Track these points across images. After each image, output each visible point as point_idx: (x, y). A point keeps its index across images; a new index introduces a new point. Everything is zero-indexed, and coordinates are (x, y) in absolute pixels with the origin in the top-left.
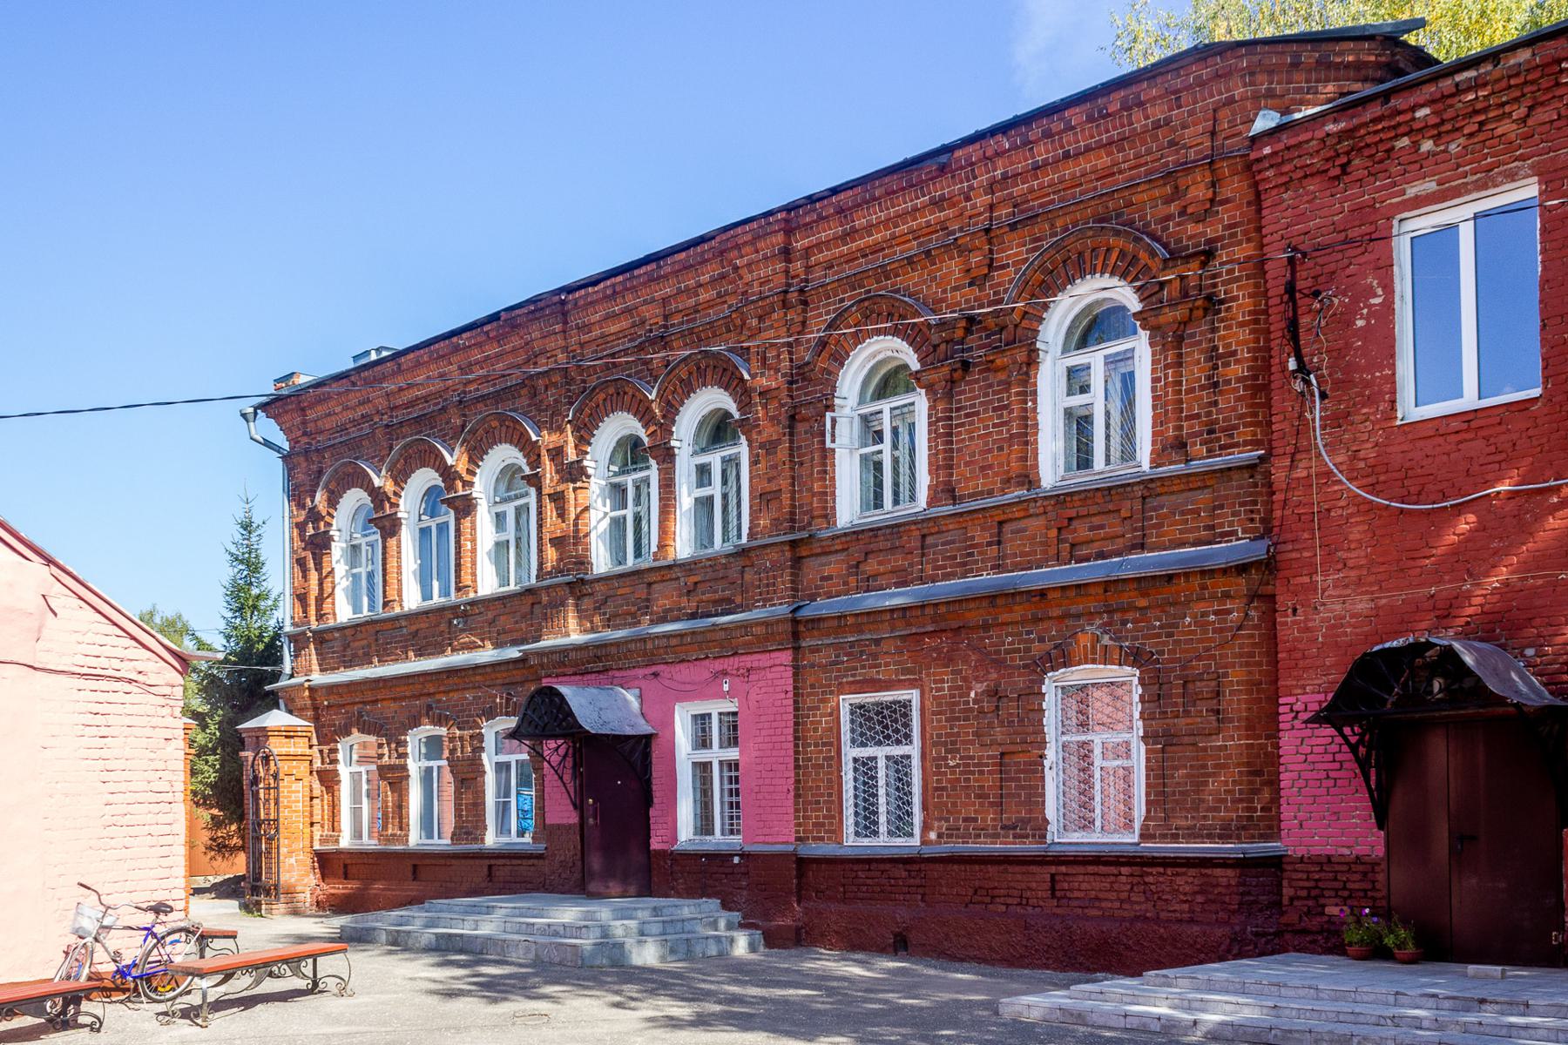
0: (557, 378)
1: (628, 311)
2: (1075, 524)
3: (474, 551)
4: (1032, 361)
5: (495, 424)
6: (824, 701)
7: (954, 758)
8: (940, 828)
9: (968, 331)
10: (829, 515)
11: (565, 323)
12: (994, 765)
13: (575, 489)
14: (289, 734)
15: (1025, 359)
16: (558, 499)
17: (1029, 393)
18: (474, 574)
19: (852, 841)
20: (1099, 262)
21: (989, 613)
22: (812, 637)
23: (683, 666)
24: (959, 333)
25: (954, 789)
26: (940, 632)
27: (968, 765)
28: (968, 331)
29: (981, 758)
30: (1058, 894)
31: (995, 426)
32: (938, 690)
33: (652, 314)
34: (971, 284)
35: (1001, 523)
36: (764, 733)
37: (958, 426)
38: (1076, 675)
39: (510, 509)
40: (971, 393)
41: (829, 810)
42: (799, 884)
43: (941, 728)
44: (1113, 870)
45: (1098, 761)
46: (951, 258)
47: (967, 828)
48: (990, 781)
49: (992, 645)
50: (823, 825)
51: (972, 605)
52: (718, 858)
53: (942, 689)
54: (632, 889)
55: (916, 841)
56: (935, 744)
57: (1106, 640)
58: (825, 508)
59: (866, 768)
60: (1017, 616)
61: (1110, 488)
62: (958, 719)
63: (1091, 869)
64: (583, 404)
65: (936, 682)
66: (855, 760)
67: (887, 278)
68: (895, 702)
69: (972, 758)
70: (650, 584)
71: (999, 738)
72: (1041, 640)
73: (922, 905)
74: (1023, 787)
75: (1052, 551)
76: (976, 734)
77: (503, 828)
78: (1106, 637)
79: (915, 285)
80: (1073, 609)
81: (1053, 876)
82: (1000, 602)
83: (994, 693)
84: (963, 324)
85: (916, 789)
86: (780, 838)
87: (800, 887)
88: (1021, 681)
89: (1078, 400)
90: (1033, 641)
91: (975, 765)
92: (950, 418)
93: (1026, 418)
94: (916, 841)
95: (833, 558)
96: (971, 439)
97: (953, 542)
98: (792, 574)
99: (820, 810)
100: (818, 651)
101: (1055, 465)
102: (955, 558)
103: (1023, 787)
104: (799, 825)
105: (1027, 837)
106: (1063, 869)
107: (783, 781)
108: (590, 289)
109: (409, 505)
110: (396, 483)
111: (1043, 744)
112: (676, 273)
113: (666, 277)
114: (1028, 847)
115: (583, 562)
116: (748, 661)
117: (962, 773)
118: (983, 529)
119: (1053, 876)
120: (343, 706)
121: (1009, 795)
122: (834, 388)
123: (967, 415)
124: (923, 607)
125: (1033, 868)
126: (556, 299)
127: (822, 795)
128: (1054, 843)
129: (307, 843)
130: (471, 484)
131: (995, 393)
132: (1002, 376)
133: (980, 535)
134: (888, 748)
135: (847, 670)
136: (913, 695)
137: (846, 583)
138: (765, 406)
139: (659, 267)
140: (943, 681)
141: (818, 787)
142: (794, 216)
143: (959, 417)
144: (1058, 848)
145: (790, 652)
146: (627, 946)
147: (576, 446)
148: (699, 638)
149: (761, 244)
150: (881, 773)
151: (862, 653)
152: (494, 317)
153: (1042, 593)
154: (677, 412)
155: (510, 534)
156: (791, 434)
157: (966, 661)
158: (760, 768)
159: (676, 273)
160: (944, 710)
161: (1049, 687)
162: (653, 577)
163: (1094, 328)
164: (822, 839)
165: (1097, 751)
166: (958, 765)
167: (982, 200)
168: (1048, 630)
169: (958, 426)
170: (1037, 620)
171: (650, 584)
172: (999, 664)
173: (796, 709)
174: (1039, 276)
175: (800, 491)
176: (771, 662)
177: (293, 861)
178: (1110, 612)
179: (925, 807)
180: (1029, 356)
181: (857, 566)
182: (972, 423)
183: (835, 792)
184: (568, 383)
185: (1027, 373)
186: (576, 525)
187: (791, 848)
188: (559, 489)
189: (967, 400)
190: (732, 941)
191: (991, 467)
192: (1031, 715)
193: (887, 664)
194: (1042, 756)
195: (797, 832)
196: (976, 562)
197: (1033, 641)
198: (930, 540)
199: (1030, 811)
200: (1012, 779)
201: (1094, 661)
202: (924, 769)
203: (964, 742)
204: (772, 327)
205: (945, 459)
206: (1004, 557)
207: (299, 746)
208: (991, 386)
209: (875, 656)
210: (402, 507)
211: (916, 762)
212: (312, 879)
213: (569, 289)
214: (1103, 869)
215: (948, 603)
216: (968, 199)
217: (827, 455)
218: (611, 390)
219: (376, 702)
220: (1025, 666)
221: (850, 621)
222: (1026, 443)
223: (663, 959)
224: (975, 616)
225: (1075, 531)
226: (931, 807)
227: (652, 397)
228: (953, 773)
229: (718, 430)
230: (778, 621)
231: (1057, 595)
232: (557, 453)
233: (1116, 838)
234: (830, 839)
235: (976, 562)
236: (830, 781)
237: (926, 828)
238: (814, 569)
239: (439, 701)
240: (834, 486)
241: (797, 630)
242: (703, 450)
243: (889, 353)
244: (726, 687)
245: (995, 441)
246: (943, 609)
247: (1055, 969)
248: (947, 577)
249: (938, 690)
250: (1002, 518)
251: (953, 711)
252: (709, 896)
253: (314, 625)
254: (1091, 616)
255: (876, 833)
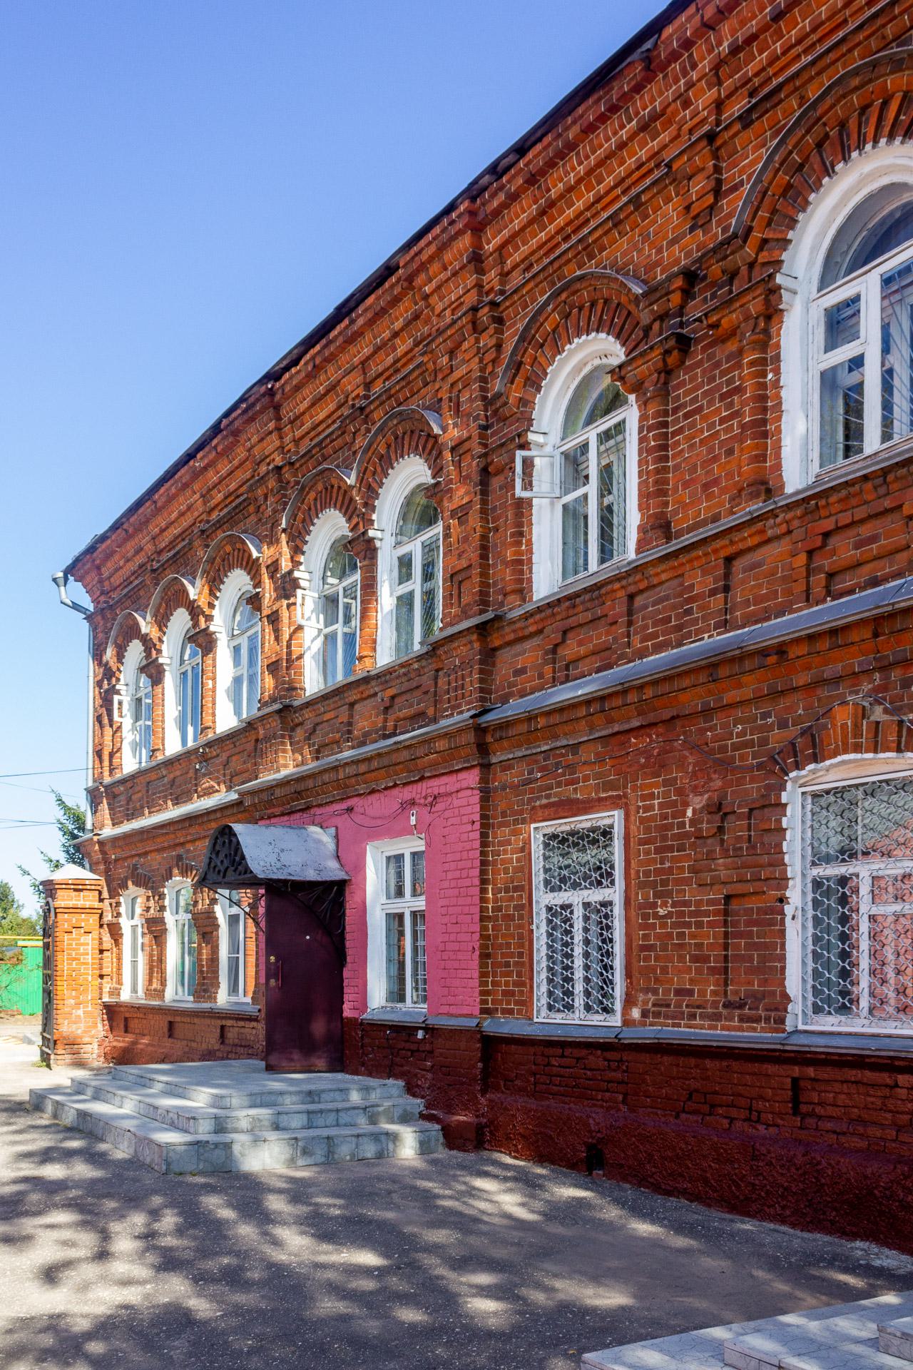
2: (834, 541)
3: (214, 690)
4: (772, 313)
5: (228, 548)
6: (516, 833)
7: (664, 904)
8: (645, 1002)
9: (687, 294)
10: (522, 589)
11: (279, 418)
12: (716, 913)
14: (78, 887)
15: (761, 308)
16: (274, 619)
17: (768, 358)
18: (214, 715)
19: (544, 1017)
20: (870, 130)
21: (710, 693)
22: (503, 749)
23: (376, 795)
24: (676, 298)
25: (664, 948)
26: (648, 723)
27: (682, 914)
28: (687, 294)
29: (699, 903)
30: (804, 1108)
31: (722, 421)
32: (648, 808)
33: (352, 384)
34: (692, 229)
35: (729, 560)
36: (450, 875)
37: (675, 433)
38: (836, 771)
39: (244, 642)
40: (691, 385)
41: (519, 975)
42: (484, 1070)
43: (649, 862)
44: (886, 1078)
45: (865, 905)
46: (668, 200)
47: (679, 1005)
48: (711, 937)
49: (716, 739)
50: (512, 993)
51: (686, 682)
52: (403, 1031)
53: (651, 808)
54: (321, 1063)
55: (616, 1020)
56: (642, 885)
57: (878, 714)
58: (520, 581)
59: (560, 915)
60: (747, 692)
61: (885, 472)
62: (671, 849)
63: (853, 1074)
65: (643, 798)
66: (549, 909)
67: (591, 257)
68: (593, 830)
69: (686, 904)
70: (352, 705)
71: (723, 874)
72: (783, 725)
73: (624, 1109)
74: (756, 946)
75: (800, 587)
76: (693, 870)
77: (234, 989)
78: (879, 710)
79: (624, 254)
80: (828, 672)
81: (795, 1081)
82: (723, 672)
83: (717, 809)
84: (679, 282)
85: (619, 949)
86: (462, 1014)
87: (486, 1073)
88: (753, 789)
90: (770, 728)
91: (691, 914)
92: (665, 424)
93: (764, 398)
94: (616, 1020)
95: (527, 645)
96: (692, 447)
97: (667, 598)
98: (481, 671)
99: (509, 974)
100: (510, 768)
101: (806, 460)
102: (668, 619)
103: (756, 946)
104: (487, 993)
105: (758, 1020)
106: (811, 1071)
107: (468, 937)
108: (293, 370)
109: (168, 653)
110: (160, 629)
111: (783, 881)
112: (371, 323)
114: (757, 1036)
115: (293, 688)
116: (436, 786)
117: (674, 925)
118: (704, 573)
119: (795, 1081)
120: (126, 858)
121: (739, 958)
122: (530, 421)
123: (686, 416)
124: (625, 692)
125: (771, 1069)
127: (512, 955)
128: (797, 1032)
129: (97, 995)
130: (209, 618)
131: (723, 374)
132: (732, 346)
133: (700, 582)
134: (586, 892)
135: (541, 789)
136: (614, 818)
137: (541, 676)
138: (458, 465)
139: (353, 322)
140: (652, 796)
141: (508, 945)
142: (476, 205)
143: (677, 421)
144: (803, 1040)
145: (476, 771)
146: (236, 1148)
148: (385, 761)
149: (448, 256)
150: (578, 925)
151: (557, 765)
152: (216, 429)
153: (780, 650)
154: (377, 496)
155: (244, 670)
156: (484, 493)
157: (682, 766)
158: (445, 920)
159: (371, 323)
160: (654, 839)
161: (792, 795)
162: (353, 696)
164: (511, 1012)
165: (865, 889)
166: (669, 915)
167: (703, 100)
168: (788, 709)
169: (675, 433)
170: (776, 694)
171: (352, 705)
172: (725, 766)
173: (484, 844)
174: (783, 178)
175: (495, 565)
176: (458, 786)
177: (80, 1012)
178: (884, 668)
179: (628, 974)
180: (767, 302)
181: (554, 651)
182: (693, 425)
183: (526, 952)
184: (282, 488)
185: (766, 331)
186: (289, 646)
187: (472, 1023)
189: (686, 393)
190: (394, 1137)
191: (716, 482)
192: (766, 839)
193: (586, 779)
194: (782, 900)
195: (484, 1002)
196: (696, 621)
197: (770, 728)
198: (639, 601)
199: (764, 982)
200: (740, 935)
201: (857, 748)
202: (628, 920)
203: (679, 882)
205: (656, 482)
206: (733, 610)
207: (89, 900)
208: (717, 365)
209: (571, 768)
210: (165, 653)
211: (618, 910)
212: (101, 1029)
213: (273, 376)
214: (869, 1075)
215: (655, 683)
216: (687, 104)
217: (522, 508)
218: (320, 486)
219: (146, 854)
220: (760, 766)
221: (542, 722)
222: (765, 435)
223: (291, 1162)
224: (692, 700)
225: (834, 552)
226: (636, 974)
227: (351, 480)
228: (663, 926)
229: (424, 509)
230: (460, 731)
231: (802, 650)
232: (274, 567)
233: (889, 1028)
234: (519, 1012)
235: (696, 621)
236: (521, 937)
237: (629, 1002)
238: (508, 661)
239: (188, 851)
240: (530, 551)
241: (483, 741)
243: (597, 362)
244: (413, 820)
245: (722, 443)
246: (649, 693)
247: (793, 1226)
248: (658, 648)
249: (648, 808)
250: (731, 550)
251: (664, 838)
252: (396, 1077)
253: (107, 780)
254: (854, 677)
255: (569, 1007)
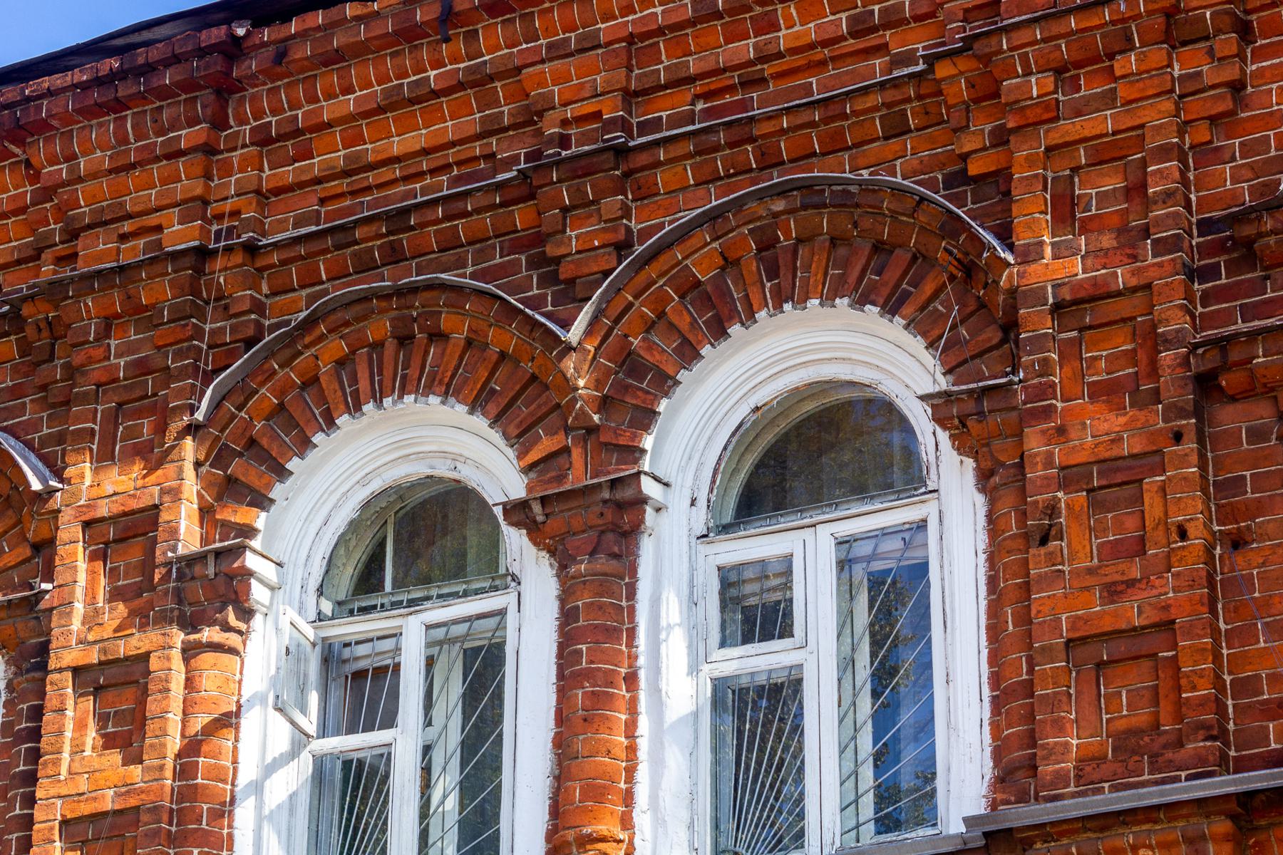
0: (160, 291)
1: (479, 81)
11: (219, 123)
13: (190, 652)
64: (260, 372)
89: (759, 660)
113: (359, 51)
126: (216, 34)
138: (1070, 352)
147: (206, 512)
163: (810, 453)
188: (122, 649)
204: (1109, 99)
218: (380, 327)
242: (725, 529)
